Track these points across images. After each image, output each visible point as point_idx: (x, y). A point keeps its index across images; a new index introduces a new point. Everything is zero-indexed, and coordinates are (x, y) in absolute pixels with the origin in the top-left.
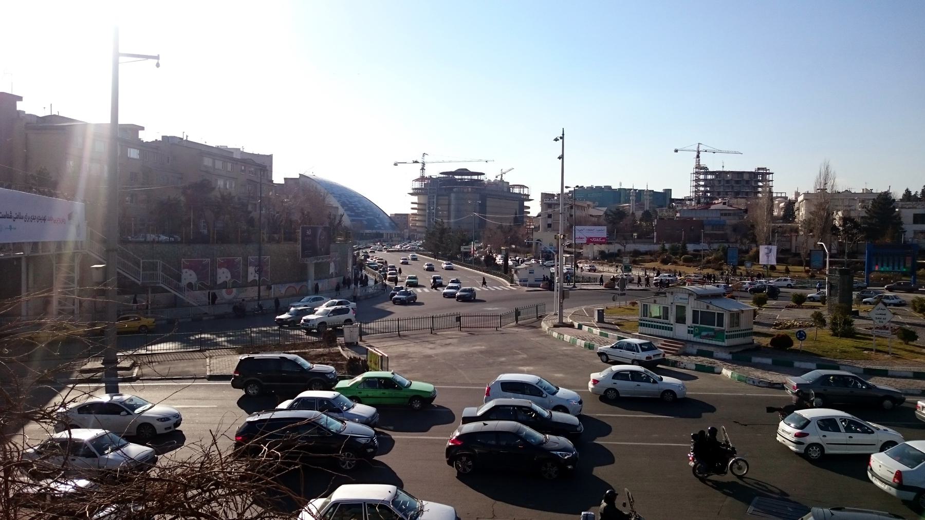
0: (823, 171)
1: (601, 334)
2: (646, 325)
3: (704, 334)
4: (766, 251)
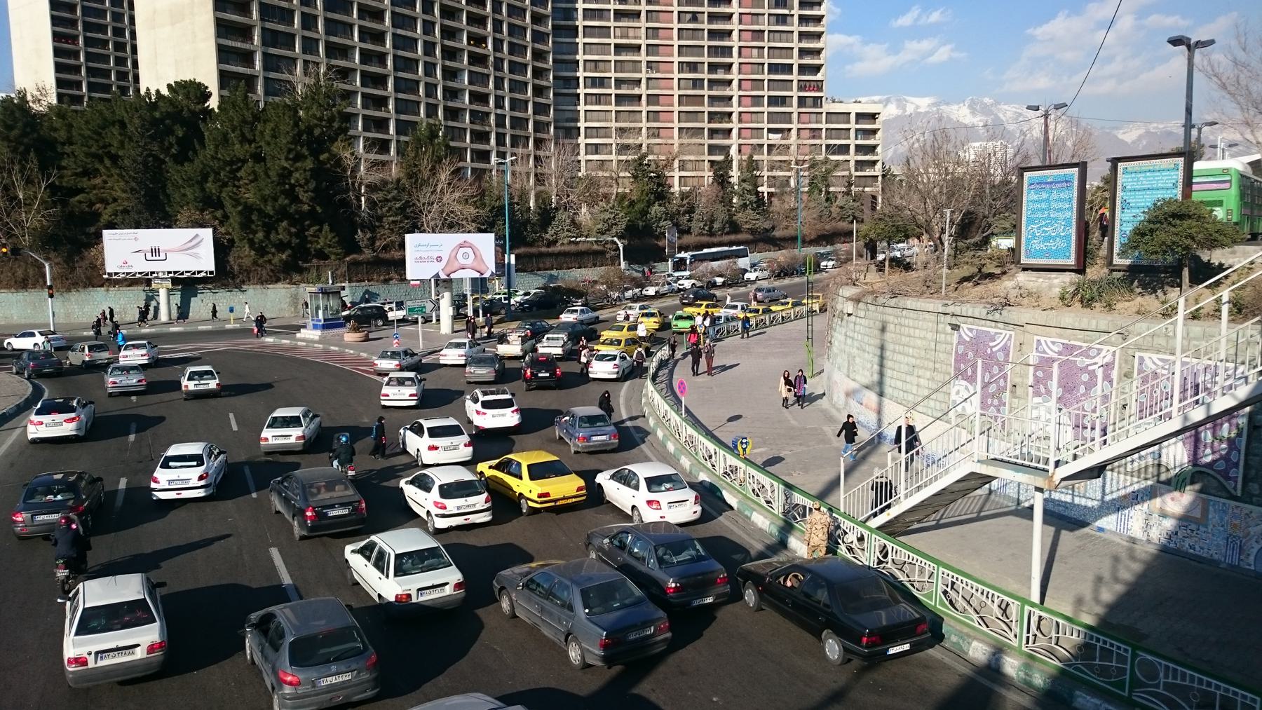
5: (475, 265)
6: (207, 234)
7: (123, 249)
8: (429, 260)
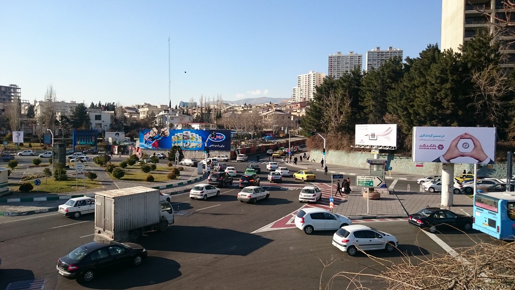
0: (49, 90)
4: (17, 134)
5: (474, 153)
6: (394, 127)
7: (363, 133)
8: (433, 147)
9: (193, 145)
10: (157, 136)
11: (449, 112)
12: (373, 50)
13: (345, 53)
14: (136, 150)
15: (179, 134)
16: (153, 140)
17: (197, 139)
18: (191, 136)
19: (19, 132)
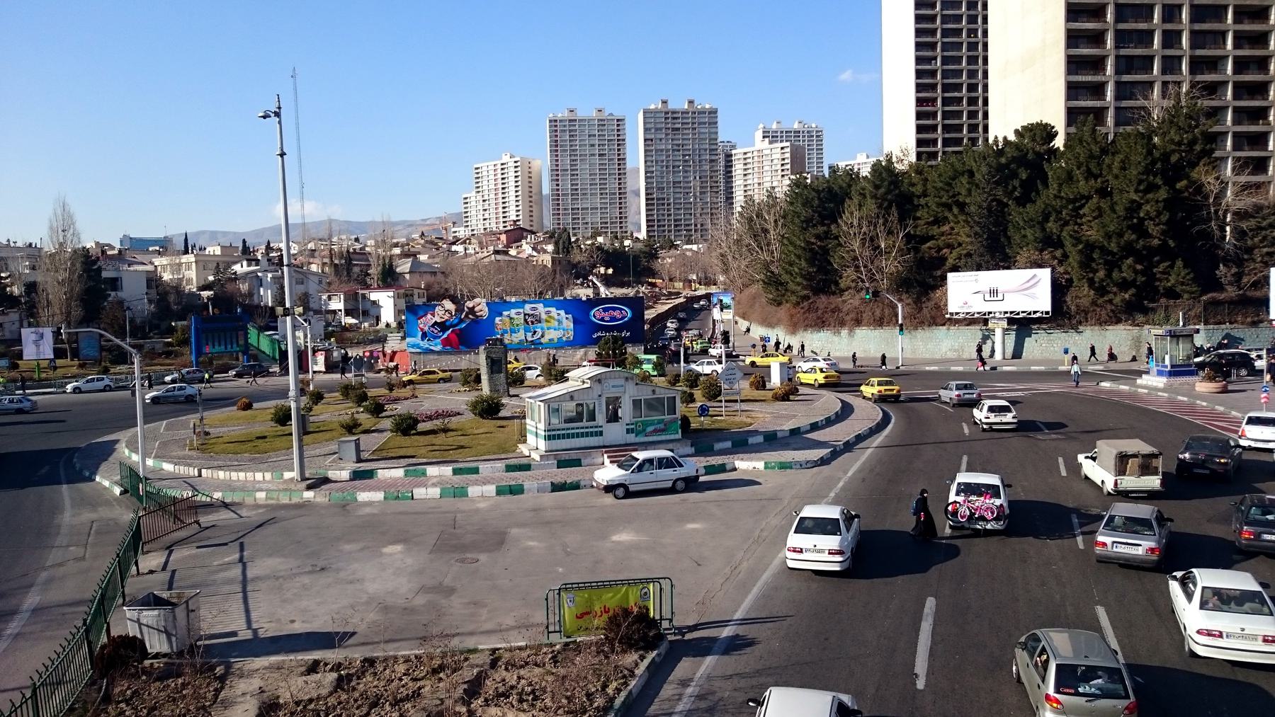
0: (59, 212)
1: (455, 472)
2: (559, 437)
3: (650, 429)
4: (33, 337)
6: (1045, 275)
7: (965, 290)
9: (552, 335)
10: (454, 320)
11: (1156, 242)
12: (652, 107)
13: (587, 111)
14: (388, 358)
15: (513, 311)
16: (444, 331)
17: (560, 322)
18: (544, 316)
19: (41, 330)
